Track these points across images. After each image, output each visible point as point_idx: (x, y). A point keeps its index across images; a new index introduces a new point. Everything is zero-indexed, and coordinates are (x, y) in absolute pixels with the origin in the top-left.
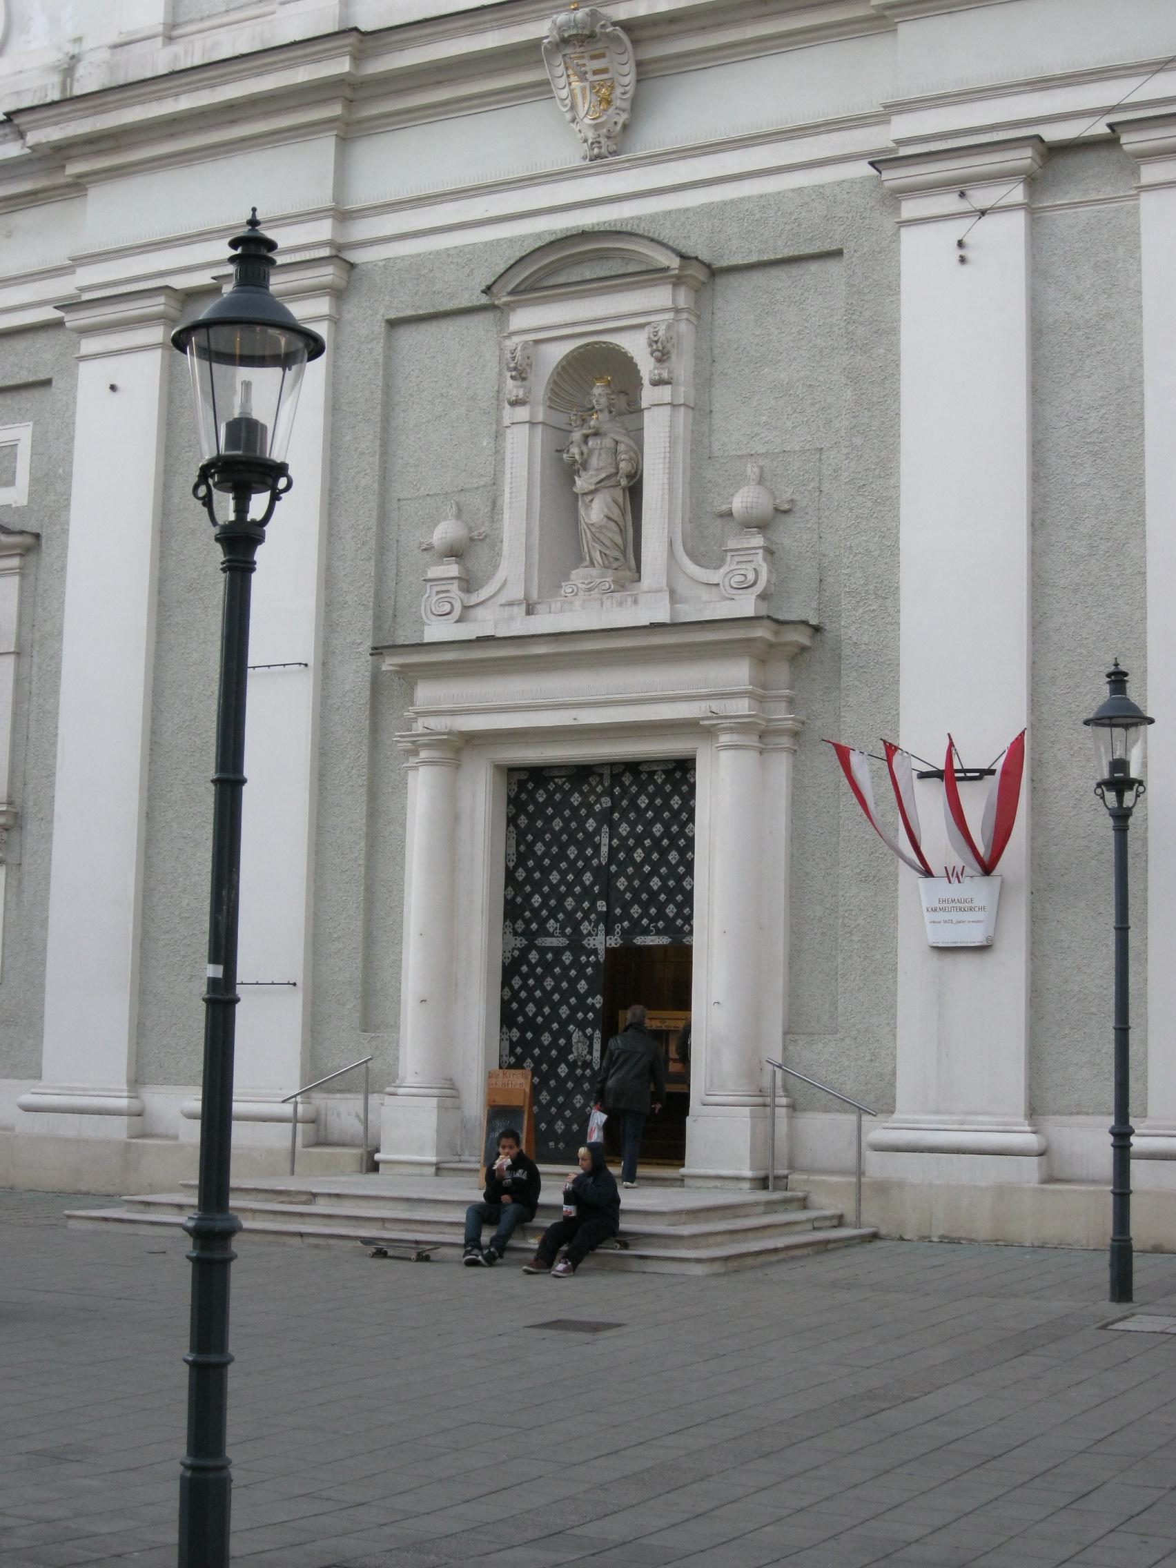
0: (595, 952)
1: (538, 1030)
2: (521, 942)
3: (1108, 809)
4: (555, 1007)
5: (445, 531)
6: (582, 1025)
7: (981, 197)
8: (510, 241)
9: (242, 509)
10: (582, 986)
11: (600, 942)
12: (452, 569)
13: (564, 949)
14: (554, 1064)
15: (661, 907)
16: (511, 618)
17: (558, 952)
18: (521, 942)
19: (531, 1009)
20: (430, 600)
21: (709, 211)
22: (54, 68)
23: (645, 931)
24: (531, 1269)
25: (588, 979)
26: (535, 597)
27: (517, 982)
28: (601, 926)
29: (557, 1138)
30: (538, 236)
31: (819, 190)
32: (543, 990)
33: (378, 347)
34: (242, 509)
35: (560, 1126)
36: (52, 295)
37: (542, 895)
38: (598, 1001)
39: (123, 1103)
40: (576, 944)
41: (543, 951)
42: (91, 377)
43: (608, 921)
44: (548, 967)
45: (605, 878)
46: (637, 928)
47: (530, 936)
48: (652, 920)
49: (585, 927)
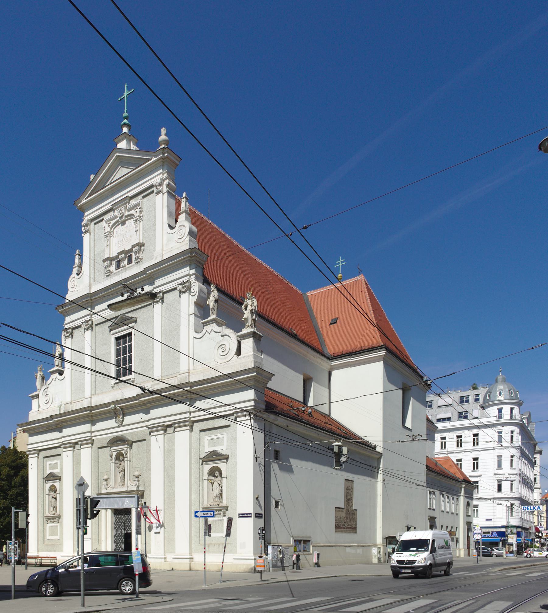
2: (116, 532)
3: (426, 440)
5: (105, 477)
6: (122, 543)
7: (159, 433)
8: (111, 436)
10: (122, 538)
11: (123, 532)
12: (105, 483)
14: (120, 548)
16: (111, 490)
17: (120, 533)
18: (116, 532)
20: (103, 487)
21: (132, 433)
22: (58, 407)
23: (129, 531)
24: (263, 598)
26: (114, 486)
27: (116, 537)
30: (114, 436)
33: (97, 451)
36: (42, 484)
38: (124, 540)
39: (189, 557)
40: (121, 533)
41: (118, 533)
42: (64, 454)
44: (119, 535)
45: (124, 524)
47: (117, 531)
49: (122, 530)
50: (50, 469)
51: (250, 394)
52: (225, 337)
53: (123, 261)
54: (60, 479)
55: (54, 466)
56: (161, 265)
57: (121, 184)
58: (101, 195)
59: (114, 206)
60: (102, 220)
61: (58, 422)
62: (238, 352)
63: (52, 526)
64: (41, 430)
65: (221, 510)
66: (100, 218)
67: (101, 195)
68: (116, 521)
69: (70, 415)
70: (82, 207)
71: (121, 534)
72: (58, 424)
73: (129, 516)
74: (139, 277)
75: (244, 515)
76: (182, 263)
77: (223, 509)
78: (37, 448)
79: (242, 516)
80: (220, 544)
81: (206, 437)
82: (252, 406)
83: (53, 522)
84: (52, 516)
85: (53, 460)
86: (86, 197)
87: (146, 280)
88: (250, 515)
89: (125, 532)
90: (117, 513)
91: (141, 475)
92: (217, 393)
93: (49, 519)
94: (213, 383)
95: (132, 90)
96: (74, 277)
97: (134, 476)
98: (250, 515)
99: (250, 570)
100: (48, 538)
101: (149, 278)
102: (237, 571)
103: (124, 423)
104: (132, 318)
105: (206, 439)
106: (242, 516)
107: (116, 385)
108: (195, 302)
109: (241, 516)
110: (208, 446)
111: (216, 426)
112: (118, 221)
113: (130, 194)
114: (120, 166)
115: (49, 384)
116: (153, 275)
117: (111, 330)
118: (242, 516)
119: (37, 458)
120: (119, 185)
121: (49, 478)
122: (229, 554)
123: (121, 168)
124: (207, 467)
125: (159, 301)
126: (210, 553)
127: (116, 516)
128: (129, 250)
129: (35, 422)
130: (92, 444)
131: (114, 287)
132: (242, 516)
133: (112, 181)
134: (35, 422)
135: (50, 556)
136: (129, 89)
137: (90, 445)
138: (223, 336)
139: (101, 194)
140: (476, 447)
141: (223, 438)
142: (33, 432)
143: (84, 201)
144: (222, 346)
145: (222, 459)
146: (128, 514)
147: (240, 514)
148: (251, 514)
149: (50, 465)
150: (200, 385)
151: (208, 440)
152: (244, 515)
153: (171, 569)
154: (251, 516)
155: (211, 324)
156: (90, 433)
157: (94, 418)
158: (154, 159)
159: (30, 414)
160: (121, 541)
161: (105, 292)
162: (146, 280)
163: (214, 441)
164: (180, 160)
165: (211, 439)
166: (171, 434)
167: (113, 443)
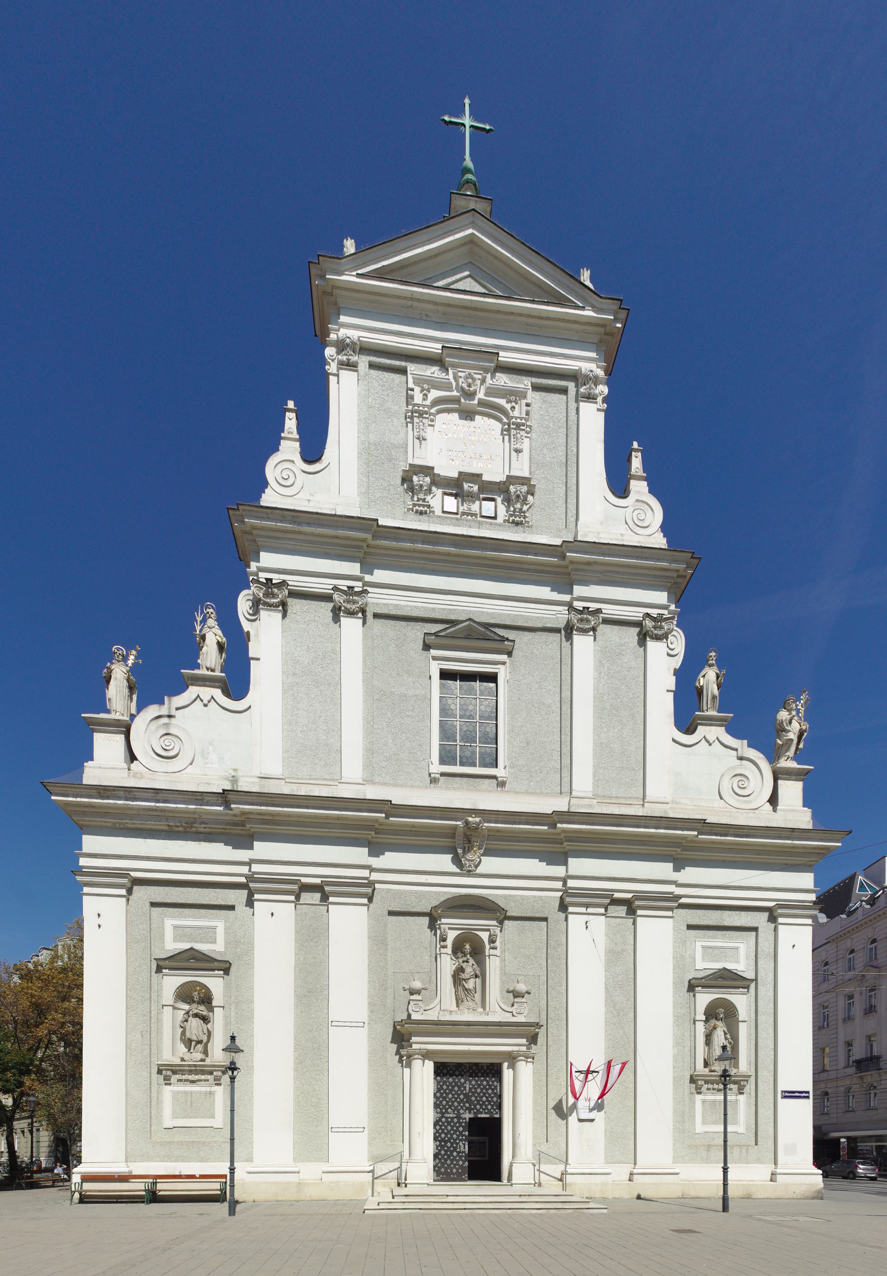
0: (465, 1119)
1: (446, 1142)
4: (452, 1135)
9: (233, 1073)
11: (467, 1116)
13: (454, 1118)
14: (452, 1152)
15: (487, 1106)
17: (452, 1118)
19: (443, 1136)
23: (481, 1113)
25: (463, 1127)
28: (467, 1111)
29: (454, 1174)
31: (540, 897)
32: (447, 1130)
34: (233, 1073)
35: (454, 1170)
37: (445, 1150)
38: (467, 1133)
40: (459, 1117)
41: (447, 1118)
43: (470, 1110)
46: (479, 1112)
48: (483, 1109)
50: (176, 939)
51: (806, 880)
52: (744, 762)
53: (469, 501)
54: (227, 971)
55: (209, 935)
56: (609, 556)
57: (476, 313)
58: (410, 303)
59: (450, 356)
60: (403, 371)
61: (243, 818)
62: (773, 800)
63: (178, 1093)
64: (151, 824)
65: (211, 1073)
66: (389, 358)
67: (410, 303)
68: (438, 1090)
69: (307, 808)
70: (335, 292)
71: (455, 1120)
72: (243, 824)
73: (482, 1081)
74: (536, 555)
75: (794, 1095)
76: (656, 576)
77: (166, 1070)
78: (133, 874)
79: (790, 1095)
80: (743, 1146)
81: (171, 921)
82: (810, 902)
83: (193, 1082)
84: (195, 1066)
85: (195, 917)
86: (359, 272)
87: (548, 572)
88: (807, 1095)
89: (472, 1116)
90: (445, 1071)
91: (529, 993)
92: (735, 862)
93: (174, 1072)
94: (746, 838)
95: (488, 127)
96: (293, 462)
97: (508, 992)
98: (807, 1095)
99: (816, 1194)
100: (168, 1123)
101: (557, 573)
102: (787, 1197)
103: (479, 870)
104: (507, 639)
105: (699, 944)
106: (790, 1095)
107: (442, 779)
108: (675, 669)
109: (786, 1094)
110: (703, 959)
111: (726, 923)
112: (456, 400)
113: (505, 357)
114: (467, 273)
115: (177, 709)
116: (576, 570)
117: (427, 647)
118: (789, 1095)
119: (124, 899)
120: (471, 312)
121: (179, 961)
122: (753, 1165)
123: (469, 279)
124: (704, 998)
125: (589, 632)
126: (711, 1163)
127: (439, 1078)
128: (490, 483)
129: (138, 794)
130: (370, 899)
131: (455, 545)
132: (789, 1095)
133: (452, 287)
134: (138, 794)
135: (197, 1174)
136: (474, 115)
137: (365, 901)
138: (741, 758)
139: (412, 298)
140: (779, 1095)
141: (215, 928)
142: (110, 821)
143: (349, 278)
144: (739, 778)
145: (738, 988)
146: (480, 1074)
147: (785, 1092)
148: (808, 1092)
149: (176, 927)
150: (716, 835)
151: (703, 947)
152: (794, 1095)
153: (635, 1196)
154: (808, 1097)
155: (716, 725)
156: (367, 871)
157: (382, 839)
158: (589, 313)
159: (86, 770)
160: (458, 1136)
161: (423, 543)
162: (548, 572)
163: (716, 951)
164: (609, 372)
165: (709, 947)
166: (618, 920)
167: (449, 908)
